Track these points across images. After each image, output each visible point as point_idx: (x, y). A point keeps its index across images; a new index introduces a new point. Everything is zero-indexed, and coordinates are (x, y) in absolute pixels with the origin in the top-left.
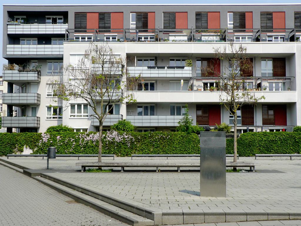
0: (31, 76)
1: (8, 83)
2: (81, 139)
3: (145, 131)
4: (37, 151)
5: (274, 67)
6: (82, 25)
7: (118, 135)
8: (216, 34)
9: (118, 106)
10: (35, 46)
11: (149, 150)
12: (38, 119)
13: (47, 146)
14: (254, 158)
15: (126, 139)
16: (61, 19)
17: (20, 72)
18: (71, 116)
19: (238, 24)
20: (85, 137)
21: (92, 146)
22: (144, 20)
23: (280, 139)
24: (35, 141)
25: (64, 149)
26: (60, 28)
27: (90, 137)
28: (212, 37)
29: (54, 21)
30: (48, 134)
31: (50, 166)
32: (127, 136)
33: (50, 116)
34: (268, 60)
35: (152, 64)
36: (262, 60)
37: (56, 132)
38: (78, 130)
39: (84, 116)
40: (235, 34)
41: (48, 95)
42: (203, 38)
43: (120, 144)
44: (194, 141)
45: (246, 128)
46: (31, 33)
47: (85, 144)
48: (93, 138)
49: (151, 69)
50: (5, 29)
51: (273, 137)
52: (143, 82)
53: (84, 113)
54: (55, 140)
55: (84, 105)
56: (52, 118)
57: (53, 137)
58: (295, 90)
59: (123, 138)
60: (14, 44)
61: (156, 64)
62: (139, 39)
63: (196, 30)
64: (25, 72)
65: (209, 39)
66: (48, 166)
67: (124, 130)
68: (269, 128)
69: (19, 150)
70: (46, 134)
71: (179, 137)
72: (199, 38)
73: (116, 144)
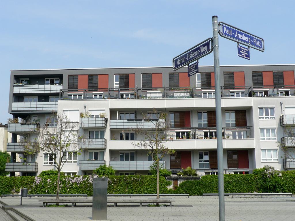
0: (30, 128)
2: (67, 182)
3: (121, 174)
5: (237, 118)
6: (75, 86)
8: (186, 91)
9: (103, 153)
10: (35, 103)
11: (124, 191)
12: (37, 165)
13: (39, 188)
14: (202, 197)
16: (58, 80)
17: (22, 125)
19: (205, 82)
21: (77, 188)
22: (125, 80)
23: (235, 180)
26: (56, 88)
27: (74, 180)
28: (183, 94)
29: (52, 83)
30: (40, 177)
31: (23, 203)
33: (47, 162)
34: (231, 112)
35: (132, 116)
36: (226, 112)
37: (47, 176)
38: (69, 174)
39: (74, 162)
40: (202, 91)
42: (175, 95)
44: (162, 183)
45: (211, 171)
46: (20, 93)
48: (77, 180)
49: (131, 122)
50: (12, 89)
51: (229, 179)
52: (140, 133)
53: (74, 159)
54: (46, 182)
56: (48, 163)
57: (44, 180)
58: (253, 138)
60: (19, 101)
61: (136, 117)
62: (122, 97)
64: (26, 125)
65: (181, 96)
66: (21, 203)
67: (104, 174)
68: (234, 171)
69: (16, 191)
70: (38, 178)
71: (150, 179)
72: (172, 95)
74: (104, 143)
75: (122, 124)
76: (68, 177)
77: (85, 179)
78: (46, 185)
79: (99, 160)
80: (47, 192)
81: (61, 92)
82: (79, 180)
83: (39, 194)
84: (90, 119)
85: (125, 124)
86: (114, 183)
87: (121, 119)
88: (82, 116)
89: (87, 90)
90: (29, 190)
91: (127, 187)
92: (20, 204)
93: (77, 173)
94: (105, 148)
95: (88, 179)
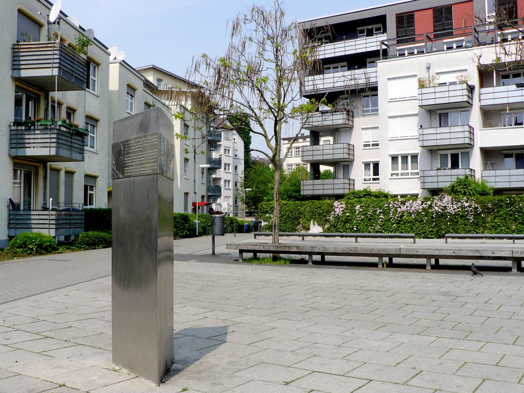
1: (310, 131)
2: (392, 210)
4: (329, 229)
7: (453, 201)
9: (467, 155)
11: (508, 228)
13: (342, 222)
15: (466, 209)
18: (392, 175)
20: (398, 206)
24: (325, 214)
25: (367, 225)
27: (405, 206)
29: (370, 33)
31: (217, 251)
32: (468, 203)
33: (369, 177)
39: (412, 174)
41: (365, 146)
43: (455, 218)
47: (398, 218)
48: (411, 207)
53: (412, 169)
54: (353, 211)
55: (402, 157)
56: (372, 180)
59: (461, 207)
63: (398, 39)
67: (465, 193)
69: (304, 228)
73: (449, 217)
74: (467, 134)
75: (505, 94)
76: (394, 201)
77: (426, 204)
78: (354, 216)
79: (460, 167)
80: (355, 229)
81: (384, 47)
82: (414, 206)
84: (438, 89)
85: (511, 94)
86: (485, 212)
87: (504, 85)
88: (422, 86)
89: (432, 37)
90: (325, 225)
91: (515, 220)
92: (210, 252)
93: (420, 194)
94: (471, 145)
95: (431, 204)
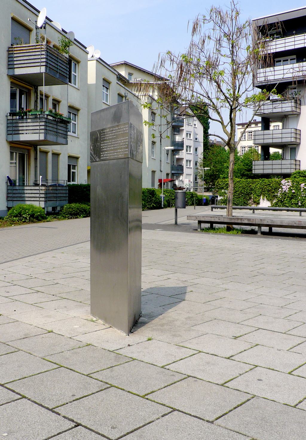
0: (287, 107)
13: (288, 197)
17: (273, 102)
24: (273, 191)
31: (178, 222)
54: (298, 189)
69: (255, 202)
78: (299, 193)
83: (288, 207)
